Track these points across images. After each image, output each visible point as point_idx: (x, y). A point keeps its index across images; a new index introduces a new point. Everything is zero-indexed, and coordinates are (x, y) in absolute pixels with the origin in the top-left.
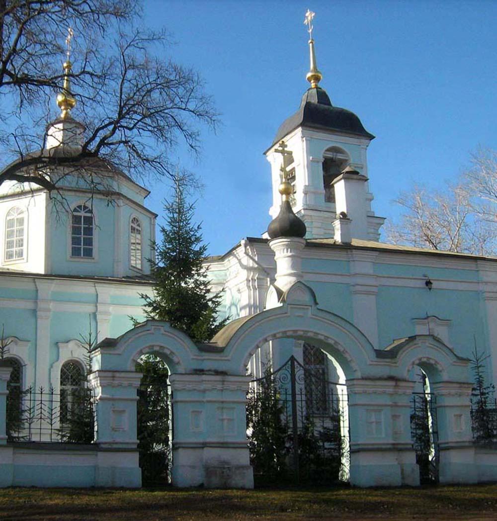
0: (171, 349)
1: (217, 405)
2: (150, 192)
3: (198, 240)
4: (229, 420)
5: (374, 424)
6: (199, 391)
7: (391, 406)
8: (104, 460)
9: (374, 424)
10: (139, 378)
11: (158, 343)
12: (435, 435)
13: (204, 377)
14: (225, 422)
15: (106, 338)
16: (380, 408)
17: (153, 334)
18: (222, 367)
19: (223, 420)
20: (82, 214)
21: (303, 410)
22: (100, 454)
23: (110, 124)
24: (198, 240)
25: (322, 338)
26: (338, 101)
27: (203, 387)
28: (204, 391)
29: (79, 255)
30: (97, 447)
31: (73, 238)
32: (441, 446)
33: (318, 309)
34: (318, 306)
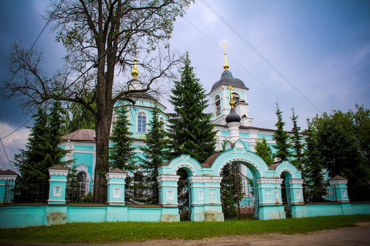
0: (191, 166)
1: (209, 189)
2: (167, 108)
3: (30, 139)
4: (269, 195)
5: (268, 196)
6: (202, 183)
7: (275, 188)
8: (165, 211)
9: (268, 196)
10: (178, 178)
11: (185, 164)
12: (290, 199)
13: (204, 177)
14: (212, 195)
15: (9, 170)
16: (269, 189)
17: (183, 160)
18: (210, 173)
19: (211, 195)
20: (142, 115)
21: (244, 190)
22: (163, 209)
23: (34, 100)
24: (30, 139)
25: (248, 162)
26: (235, 76)
27: (205, 181)
28: (204, 183)
29: (141, 131)
30: (162, 206)
31: (139, 121)
32: (260, 205)
33: (247, 150)
34: (247, 149)
